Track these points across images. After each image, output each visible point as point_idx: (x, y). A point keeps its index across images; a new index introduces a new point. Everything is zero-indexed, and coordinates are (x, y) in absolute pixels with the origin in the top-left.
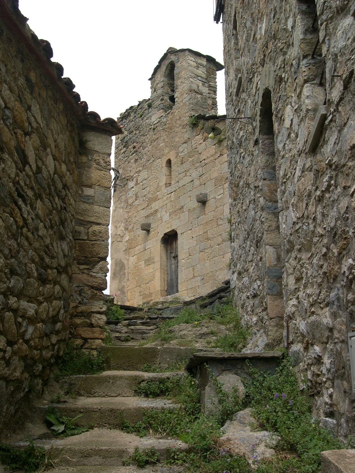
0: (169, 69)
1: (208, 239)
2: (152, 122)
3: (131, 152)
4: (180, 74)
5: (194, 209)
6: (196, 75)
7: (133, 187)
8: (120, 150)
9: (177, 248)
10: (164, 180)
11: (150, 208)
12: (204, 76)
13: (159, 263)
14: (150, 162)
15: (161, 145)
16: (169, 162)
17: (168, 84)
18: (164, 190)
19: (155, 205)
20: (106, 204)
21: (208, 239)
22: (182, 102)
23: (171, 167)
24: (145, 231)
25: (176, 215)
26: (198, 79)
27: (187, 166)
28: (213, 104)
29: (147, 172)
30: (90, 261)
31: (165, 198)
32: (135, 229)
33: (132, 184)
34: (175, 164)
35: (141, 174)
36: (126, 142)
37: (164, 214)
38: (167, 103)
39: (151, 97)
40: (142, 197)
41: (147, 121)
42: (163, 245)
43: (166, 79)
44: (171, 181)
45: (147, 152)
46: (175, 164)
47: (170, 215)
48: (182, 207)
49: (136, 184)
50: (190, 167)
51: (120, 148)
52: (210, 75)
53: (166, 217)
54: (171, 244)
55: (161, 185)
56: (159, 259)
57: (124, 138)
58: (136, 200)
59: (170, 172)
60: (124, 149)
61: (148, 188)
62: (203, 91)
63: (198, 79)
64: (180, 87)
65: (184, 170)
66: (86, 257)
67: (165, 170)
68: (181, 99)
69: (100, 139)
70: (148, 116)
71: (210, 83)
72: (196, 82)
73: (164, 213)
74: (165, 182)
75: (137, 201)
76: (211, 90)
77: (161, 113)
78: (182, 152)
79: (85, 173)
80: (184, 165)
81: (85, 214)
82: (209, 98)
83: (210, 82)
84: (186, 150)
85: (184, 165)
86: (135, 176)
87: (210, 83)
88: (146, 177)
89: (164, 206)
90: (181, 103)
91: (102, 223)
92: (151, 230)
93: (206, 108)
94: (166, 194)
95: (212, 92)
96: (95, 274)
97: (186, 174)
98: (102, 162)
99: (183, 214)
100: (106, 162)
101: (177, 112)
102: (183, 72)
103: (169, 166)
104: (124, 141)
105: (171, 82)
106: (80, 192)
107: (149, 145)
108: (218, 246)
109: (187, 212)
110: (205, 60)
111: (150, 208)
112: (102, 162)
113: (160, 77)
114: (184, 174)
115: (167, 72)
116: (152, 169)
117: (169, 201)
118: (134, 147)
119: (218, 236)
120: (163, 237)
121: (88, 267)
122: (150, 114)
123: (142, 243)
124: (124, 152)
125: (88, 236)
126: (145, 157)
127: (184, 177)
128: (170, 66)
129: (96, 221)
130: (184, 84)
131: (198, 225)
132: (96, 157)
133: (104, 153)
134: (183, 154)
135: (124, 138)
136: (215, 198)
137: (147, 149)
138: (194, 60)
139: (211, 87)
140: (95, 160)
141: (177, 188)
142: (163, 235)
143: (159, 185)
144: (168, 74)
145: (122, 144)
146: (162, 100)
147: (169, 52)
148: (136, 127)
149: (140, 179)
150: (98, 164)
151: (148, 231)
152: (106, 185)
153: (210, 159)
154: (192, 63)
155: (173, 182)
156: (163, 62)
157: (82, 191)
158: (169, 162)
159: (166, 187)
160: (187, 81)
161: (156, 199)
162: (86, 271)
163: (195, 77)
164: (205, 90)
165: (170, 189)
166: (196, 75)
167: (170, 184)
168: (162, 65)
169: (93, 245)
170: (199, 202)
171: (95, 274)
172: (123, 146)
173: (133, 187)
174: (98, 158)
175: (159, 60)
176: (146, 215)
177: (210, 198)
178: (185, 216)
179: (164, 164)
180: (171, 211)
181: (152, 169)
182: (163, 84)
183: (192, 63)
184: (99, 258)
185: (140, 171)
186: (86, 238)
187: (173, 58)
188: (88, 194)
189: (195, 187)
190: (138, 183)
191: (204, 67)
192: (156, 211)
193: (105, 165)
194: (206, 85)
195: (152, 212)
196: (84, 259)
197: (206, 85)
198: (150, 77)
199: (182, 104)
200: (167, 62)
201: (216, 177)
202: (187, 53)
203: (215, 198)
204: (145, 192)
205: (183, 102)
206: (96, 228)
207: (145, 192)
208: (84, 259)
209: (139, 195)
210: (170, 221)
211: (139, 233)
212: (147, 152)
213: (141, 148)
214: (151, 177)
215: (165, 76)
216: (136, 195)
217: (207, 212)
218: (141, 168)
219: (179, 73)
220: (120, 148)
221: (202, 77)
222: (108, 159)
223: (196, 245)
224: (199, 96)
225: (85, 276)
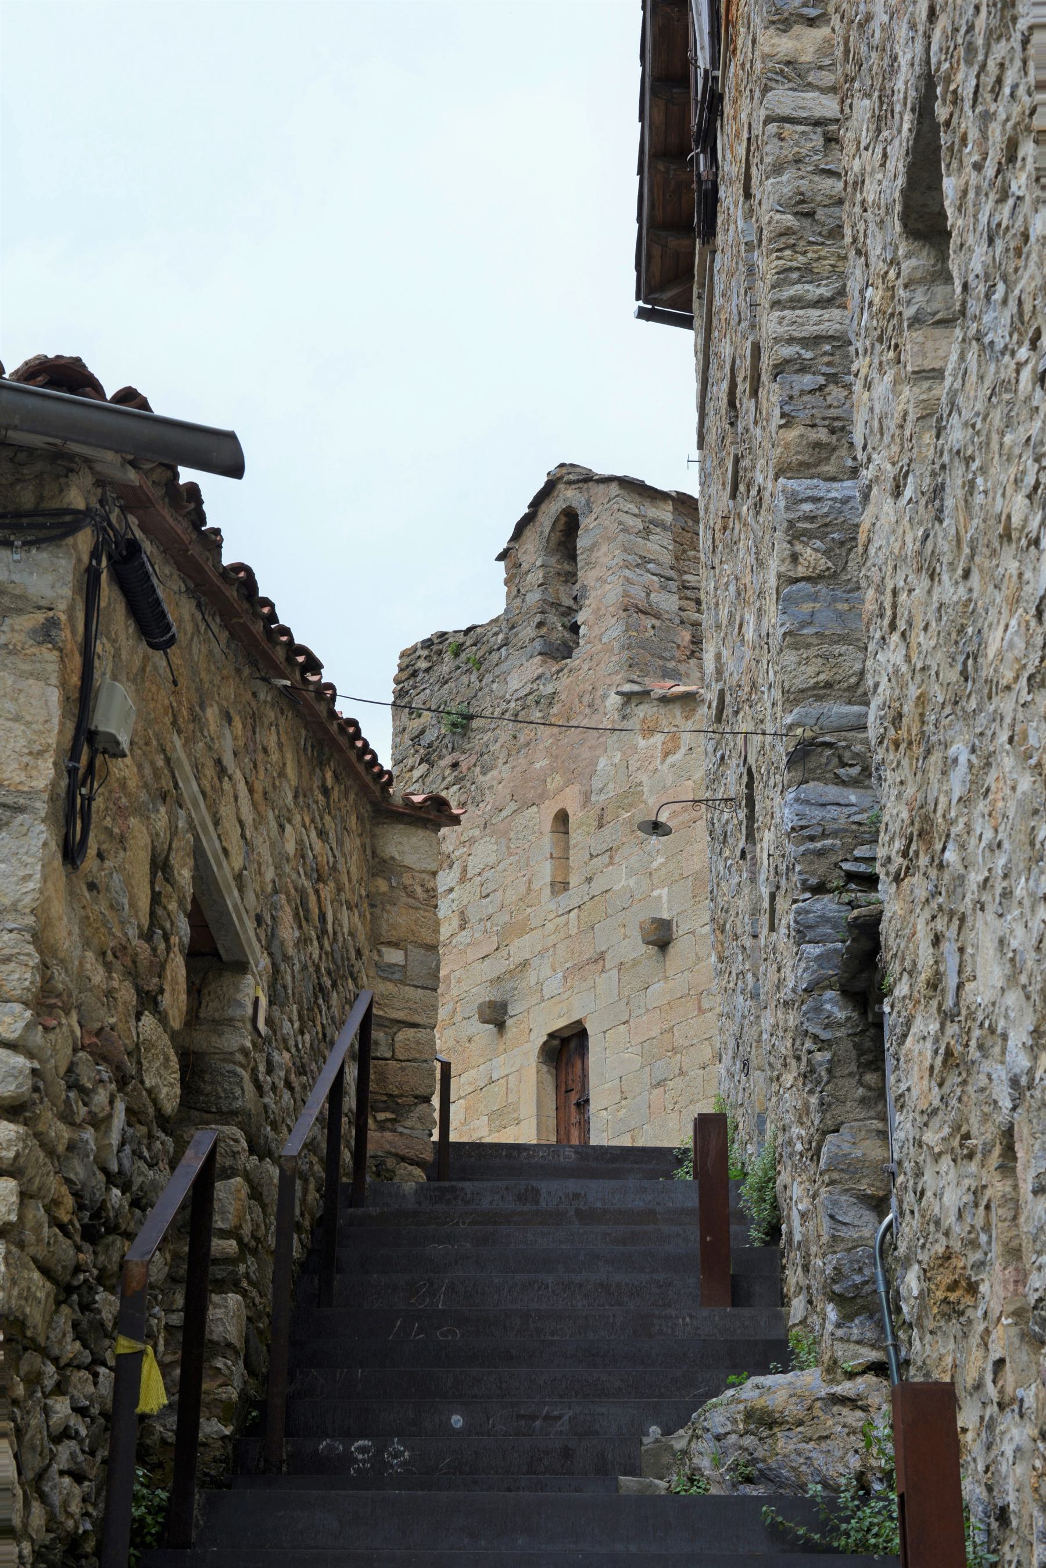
0: (562, 528)
1: (674, 1050)
2: (510, 691)
3: (444, 778)
4: (595, 554)
5: (636, 962)
6: (641, 557)
7: (451, 890)
8: (411, 770)
9: (585, 1076)
10: (546, 872)
11: (505, 953)
12: (667, 559)
13: (534, 1121)
14: (504, 814)
15: (537, 766)
16: (562, 818)
17: (559, 574)
18: (547, 904)
19: (522, 947)
20: (429, 983)
21: (674, 1050)
22: (600, 640)
23: (567, 833)
24: (491, 1026)
25: (583, 979)
26: (648, 571)
27: (609, 835)
28: (693, 643)
29: (496, 843)
30: (397, 1104)
31: (550, 926)
32: (458, 1018)
33: (449, 879)
34: (580, 825)
35: (479, 848)
36: (430, 745)
37: (549, 975)
38: (554, 636)
39: (506, 611)
40: (481, 920)
41: (495, 686)
42: (545, 1068)
43: (553, 561)
44: (567, 875)
45: (495, 783)
46: (580, 825)
47: (565, 978)
48: (602, 956)
49: (463, 879)
50: (624, 839)
51: (410, 762)
52: (684, 551)
53: (553, 986)
54: (569, 1063)
55: (536, 886)
56: (533, 1110)
57: (423, 732)
58: (462, 928)
59: (567, 848)
60: (424, 767)
61: (499, 894)
62: (664, 606)
63: (648, 571)
64: (593, 594)
65: (605, 847)
66: (390, 1096)
67: (547, 842)
68: (596, 631)
69: (414, 840)
70: (497, 671)
71: (686, 577)
72: (641, 579)
73: (546, 971)
74: (548, 879)
75: (464, 933)
76: (688, 599)
77: (534, 666)
78: (601, 790)
79: (385, 915)
80: (606, 830)
81: (386, 1005)
82: (682, 622)
83: (685, 572)
84: (611, 786)
85: (607, 832)
86: (457, 853)
87: (686, 577)
88: (492, 859)
89: (547, 950)
90: (596, 642)
91: (421, 1022)
92: (509, 1022)
93: (673, 658)
94: (552, 916)
95: (692, 604)
96: (406, 1131)
97: (611, 857)
98: (419, 890)
99: (603, 975)
100: (428, 891)
101: (586, 667)
102: (604, 549)
103: (562, 829)
104: (422, 743)
105: (567, 567)
106: (376, 958)
107: (500, 761)
108: (701, 1071)
109: (616, 971)
110: (671, 508)
111: (505, 953)
112: (419, 890)
113: (532, 555)
114: (605, 858)
115: (557, 536)
116: (512, 835)
117: (562, 935)
118: (455, 765)
119: (701, 1042)
120: (545, 1043)
121: (392, 1116)
122: (504, 667)
123: (482, 1061)
124: (423, 777)
125: (393, 1051)
126: (489, 798)
127: (607, 866)
128: (563, 519)
129: (408, 1019)
130: (608, 587)
131: (648, 1010)
132: (407, 879)
133: (423, 872)
134: (603, 797)
135: (423, 732)
136: (693, 933)
137: (495, 772)
138: (636, 511)
139: (687, 588)
140: (405, 888)
141: (586, 898)
142: (545, 1038)
143: (533, 886)
144: (560, 544)
145: (417, 751)
146: (540, 625)
147: (560, 479)
148: (458, 700)
149: (474, 865)
150: (411, 895)
151: (501, 1026)
152: (428, 940)
153: (681, 818)
154: (630, 521)
155: (574, 880)
156: (543, 507)
157: (380, 955)
158: (562, 818)
159: (552, 893)
160: (614, 578)
161: (522, 929)
162: (389, 1125)
163: (638, 565)
164: (668, 602)
165: (566, 900)
166: (641, 557)
167: (565, 886)
168: (540, 514)
169: (403, 1069)
170: (649, 943)
171: (406, 1131)
172: (418, 758)
173: (451, 890)
174: (410, 882)
175: (530, 499)
176: (495, 975)
177: (680, 933)
178: (607, 982)
179: (547, 825)
180: (568, 965)
181: (512, 835)
182: (544, 577)
183: (630, 521)
184: (416, 1097)
185: (472, 841)
186: (389, 1055)
187: (568, 496)
188: (393, 961)
189: (639, 897)
190: (469, 876)
191: (665, 528)
192: (525, 964)
193: (425, 896)
194: (673, 586)
195: (512, 967)
196: (385, 1098)
197: (673, 586)
198: (502, 545)
199: (600, 647)
200: (552, 509)
201: (697, 873)
202: (614, 489)
203: (693, 933)
204: (489, 906)
205: (604, 640)
206: (404, 1035)
207: (489, 906)
208: (385, 1098)
209: (472, 915)
210: (566, 996)
211: (471, 1030)
212: (495, 783)
213: (478, 769)
214: (508, 862)
215: (549, 551)
216: (462, 913)
217: (670, 972)
218: (477, 832)
219: (591, 549)
220: (410, 762)
221: (658, 564)
222: (431, 884)
223: (642, 1067)
224: (649, 622)
225: (388, 1134)
